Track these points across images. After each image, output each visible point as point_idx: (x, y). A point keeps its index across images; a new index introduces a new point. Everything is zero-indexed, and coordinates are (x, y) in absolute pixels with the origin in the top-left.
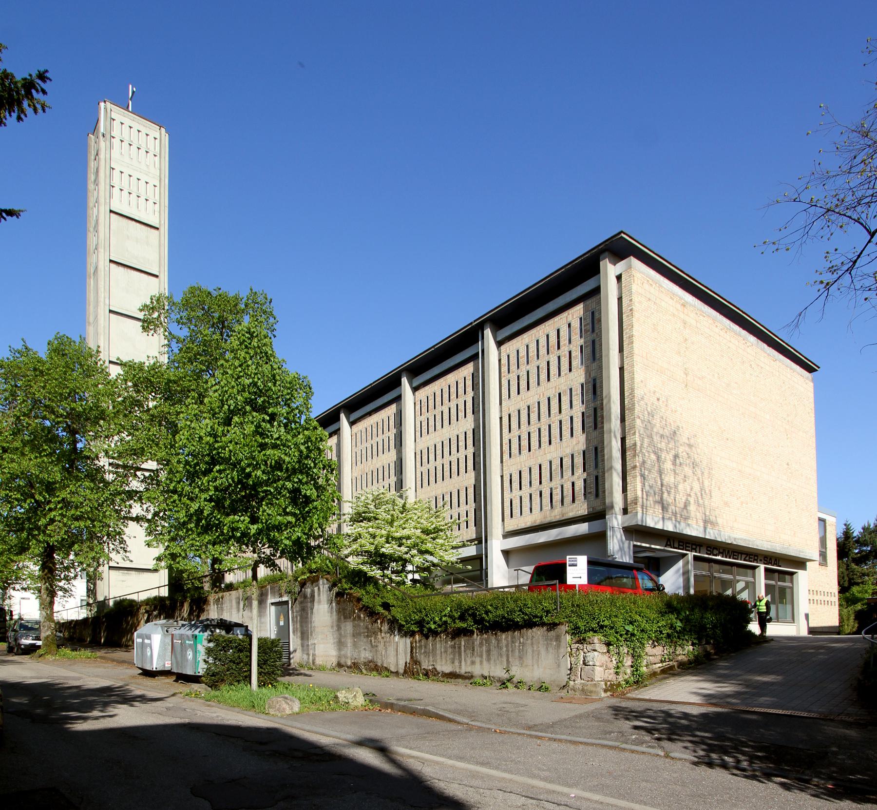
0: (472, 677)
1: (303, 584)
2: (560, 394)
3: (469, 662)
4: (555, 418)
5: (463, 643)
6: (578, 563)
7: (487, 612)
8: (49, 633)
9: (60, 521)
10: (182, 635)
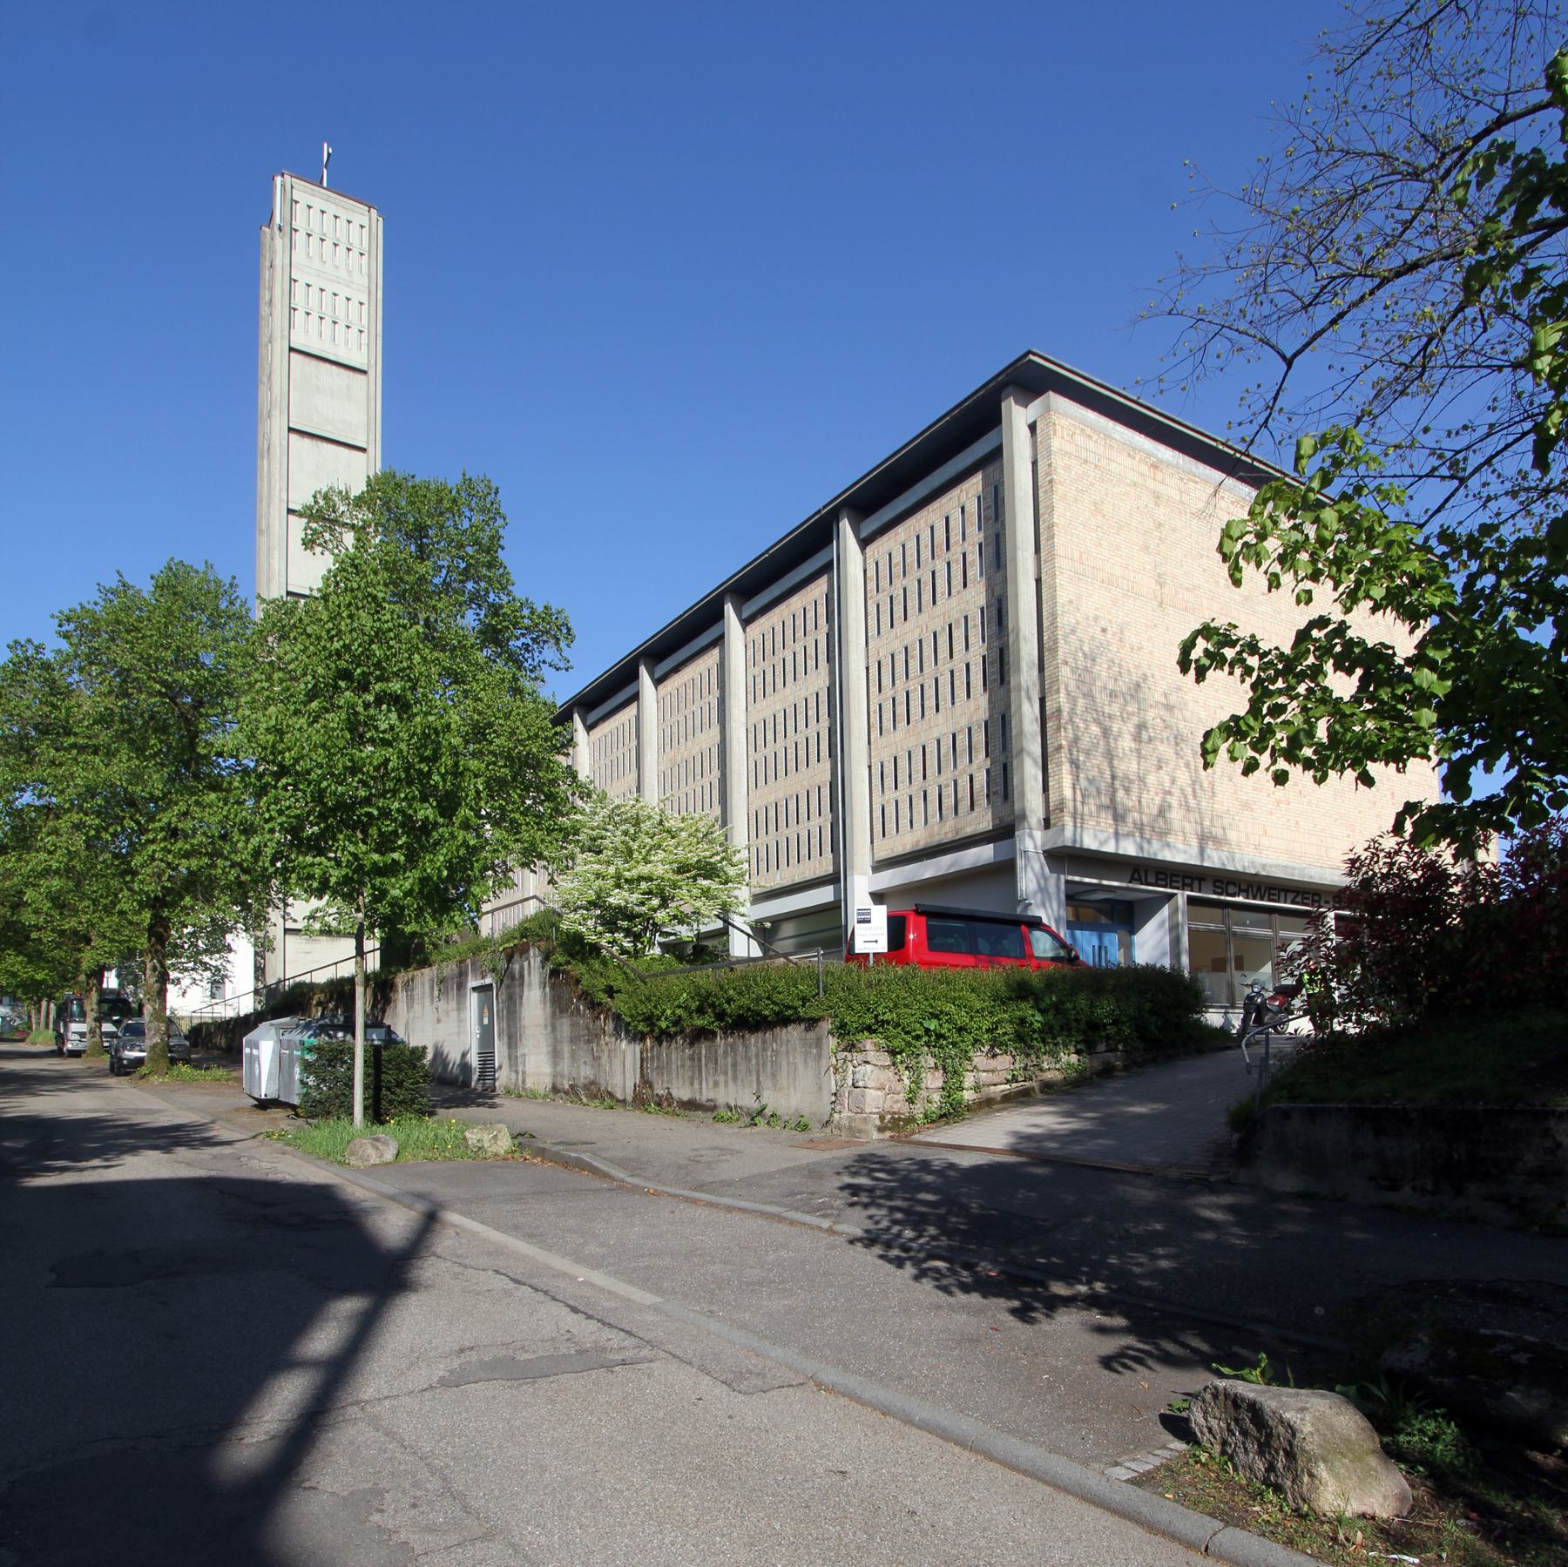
0: (714, 1108)
1: (510, 958)
2: (950, 626)
3: (711, 1084)
4: (945, 667)
5: (704, 1052)
6: (873, 917)
7: (729, 1001)
8: (157, 1040)
9: (162, 860)
10: (289, 1041)
